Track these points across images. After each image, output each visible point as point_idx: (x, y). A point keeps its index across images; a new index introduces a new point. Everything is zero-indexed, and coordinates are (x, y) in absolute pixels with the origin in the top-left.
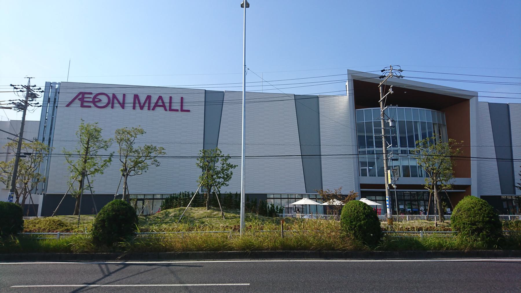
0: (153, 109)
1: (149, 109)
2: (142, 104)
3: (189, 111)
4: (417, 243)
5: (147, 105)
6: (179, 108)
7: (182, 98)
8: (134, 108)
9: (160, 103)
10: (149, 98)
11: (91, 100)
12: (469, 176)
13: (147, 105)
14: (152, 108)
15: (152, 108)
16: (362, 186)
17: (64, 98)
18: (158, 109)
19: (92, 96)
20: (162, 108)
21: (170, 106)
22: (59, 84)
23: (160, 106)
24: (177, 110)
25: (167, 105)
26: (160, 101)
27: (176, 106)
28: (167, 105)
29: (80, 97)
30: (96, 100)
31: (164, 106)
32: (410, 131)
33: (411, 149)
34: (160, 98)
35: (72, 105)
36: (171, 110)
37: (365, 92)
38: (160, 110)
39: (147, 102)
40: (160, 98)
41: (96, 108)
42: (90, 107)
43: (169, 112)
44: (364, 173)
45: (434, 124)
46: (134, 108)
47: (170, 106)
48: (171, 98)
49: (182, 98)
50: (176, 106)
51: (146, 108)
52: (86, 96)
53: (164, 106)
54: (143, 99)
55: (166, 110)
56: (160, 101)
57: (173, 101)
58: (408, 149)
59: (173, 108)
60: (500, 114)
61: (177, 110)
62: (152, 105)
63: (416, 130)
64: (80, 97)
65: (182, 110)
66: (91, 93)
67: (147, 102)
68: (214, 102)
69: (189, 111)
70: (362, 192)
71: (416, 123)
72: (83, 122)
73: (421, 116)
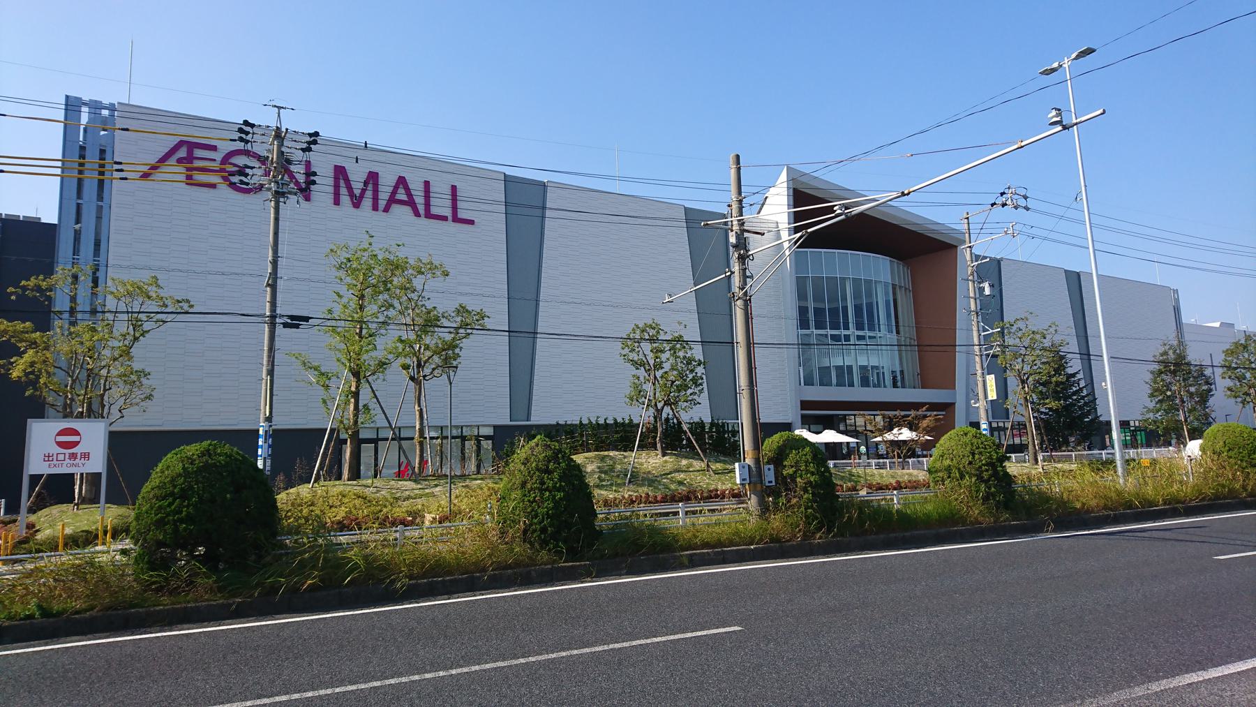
0: (386, 210)
1: (375, 208)
2: (357, 192)
3: (471, 222)
4: (888, 513)
5: (369, 194)
6: (448, 212)
7: (454, 188)
8: (337, 202)
9: (401, 195)
10: (373, 178)
11: (215, 165)
12: (952, 385)
13: (369, 194)
14: (382, 204)
15: (382, 204)
16: (805, 405)
17: (133, 151)
18: (396, 208)
19: (218, 156)
20: (407, 210)
21: (427, 205)
22: (112, 108)
23: (401, 202)
24: (444, 218)
25: (420, 200)
26: (401, 190)
27: (441, 206)
28: (420, 200)
29: (182, 153)
30: (230, 168)
31: (411, 203)
32: (869, 294)
33: (872, 334)
34: (402, 181)
35: (157, 176)
36: (429, 215)
37: (830, 226)
38: (402, 213)
39: (342, 183)
40: (402, 181)
41: (230, 190)
42: (213, 186)
43: (423, 221)
44: (809, 382)
45: (894, 287)
46: (337, 202)
47: (427, 205)
48: (427, 184)
49: (454, 188)
50: (441, 206)
51: (367, 202)
52: (199, 153)
53: (411, 203)
54: (357, 176)
55: (417, 214)
56: (401, 190)
57: (432, 189)
58: (868, 333)
59: (434, 211)
60: (992, 270)
61: (444, 218)
62: (384, 197)
63: (844, 299)
64: (182, 153)
65: (456, 219)
66: (214, 148)
67: (342, 183)
68: (526, 202)
69: (471, 222)
70: (803, 416)
71: (843, 280)
72: (372, 240)
73: (877, 269)
